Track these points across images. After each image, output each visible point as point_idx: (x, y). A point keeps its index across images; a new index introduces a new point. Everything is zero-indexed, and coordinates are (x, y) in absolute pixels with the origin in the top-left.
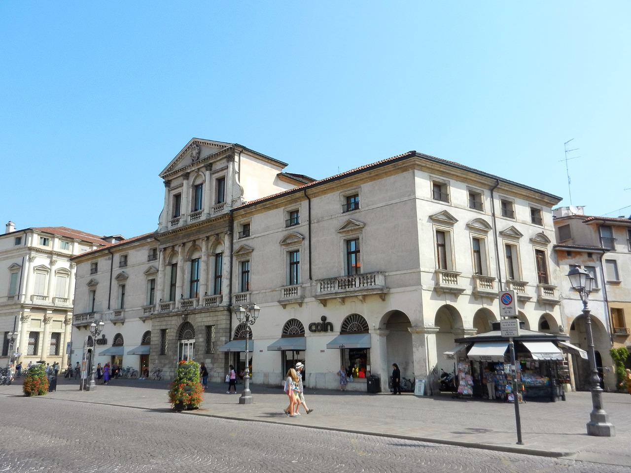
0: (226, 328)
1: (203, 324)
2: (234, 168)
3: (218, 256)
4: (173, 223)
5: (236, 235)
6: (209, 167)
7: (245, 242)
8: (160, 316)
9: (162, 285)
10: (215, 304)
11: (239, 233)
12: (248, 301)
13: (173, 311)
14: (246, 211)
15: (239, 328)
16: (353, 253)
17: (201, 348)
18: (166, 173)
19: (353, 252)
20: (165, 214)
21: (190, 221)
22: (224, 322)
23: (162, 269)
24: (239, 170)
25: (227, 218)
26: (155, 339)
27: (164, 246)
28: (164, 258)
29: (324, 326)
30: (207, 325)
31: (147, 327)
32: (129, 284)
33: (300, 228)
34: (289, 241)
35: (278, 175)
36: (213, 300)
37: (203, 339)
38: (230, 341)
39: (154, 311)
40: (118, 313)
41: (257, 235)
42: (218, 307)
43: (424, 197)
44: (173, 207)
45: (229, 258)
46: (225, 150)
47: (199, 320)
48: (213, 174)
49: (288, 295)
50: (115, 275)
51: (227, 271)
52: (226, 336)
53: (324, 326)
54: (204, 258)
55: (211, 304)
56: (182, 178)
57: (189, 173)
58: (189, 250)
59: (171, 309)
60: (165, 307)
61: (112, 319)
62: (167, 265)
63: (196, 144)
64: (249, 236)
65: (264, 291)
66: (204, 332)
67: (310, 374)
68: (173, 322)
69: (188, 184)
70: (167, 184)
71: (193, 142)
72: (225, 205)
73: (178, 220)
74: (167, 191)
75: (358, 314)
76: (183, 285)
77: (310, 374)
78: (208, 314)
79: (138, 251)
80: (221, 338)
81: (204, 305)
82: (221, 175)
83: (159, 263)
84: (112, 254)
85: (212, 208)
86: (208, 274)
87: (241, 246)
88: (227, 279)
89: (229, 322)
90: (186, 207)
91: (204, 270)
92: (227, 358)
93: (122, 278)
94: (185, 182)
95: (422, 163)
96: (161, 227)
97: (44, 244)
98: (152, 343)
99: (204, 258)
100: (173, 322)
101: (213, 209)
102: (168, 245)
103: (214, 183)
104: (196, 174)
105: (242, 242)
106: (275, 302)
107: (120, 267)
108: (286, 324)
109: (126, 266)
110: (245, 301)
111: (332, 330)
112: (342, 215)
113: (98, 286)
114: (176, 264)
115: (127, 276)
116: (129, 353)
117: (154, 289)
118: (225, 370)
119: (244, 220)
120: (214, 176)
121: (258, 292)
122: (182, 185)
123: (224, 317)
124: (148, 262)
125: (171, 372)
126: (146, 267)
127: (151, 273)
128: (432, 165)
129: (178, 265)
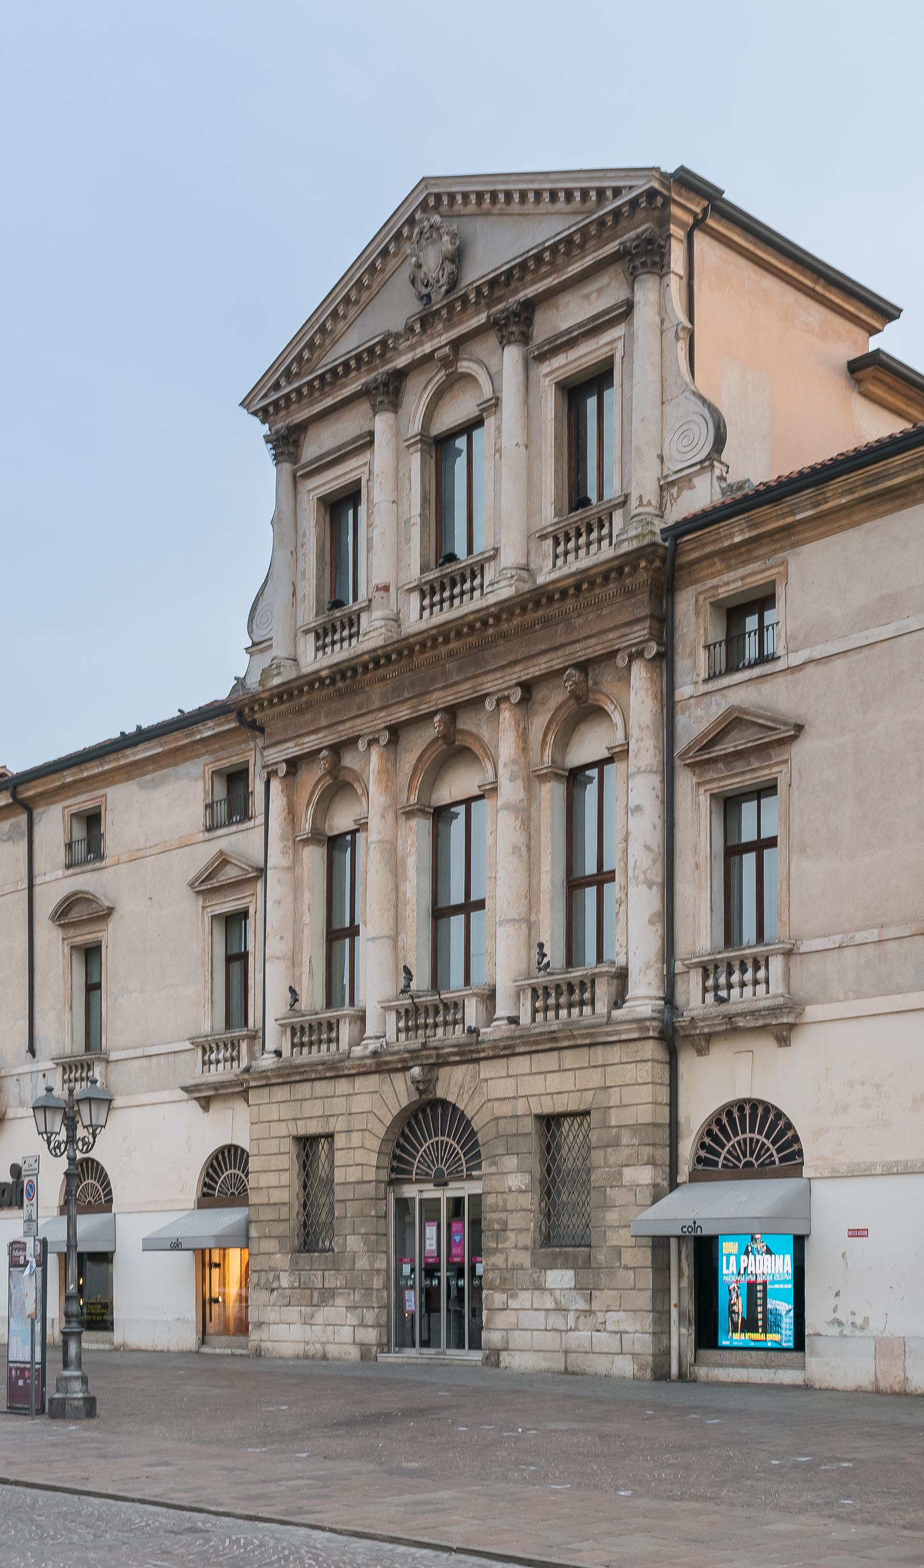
0: (655, 1125)
1: (521, 1107)
2: (663, 310)
4: (324, 634)
5: (693, 663)
6: (516, 324)
7: (742, 692)
8: (289, 1076)
9: (289, 937)
10: (587, 1010)
11: (707, 647)
12: (777, 987)
13: (357, 1051)
14: (755, 526)
15: (212, 1165)
16: (590, 884)
17: (515, 1221)
18: (277, 386)
19: (457, 909)
20: (279, 596)
21: (415, 618)
22: (646, 1093)
23: (285, 862)
24: (691, 319)
25: (643, 576)
26: (273, 1178)
27: (291, 750)
30: (302, 1132)
31: (230, 1126)
32: (114, 939)
34: (727, 747)
36: (577, 992)
37: (526, 1179)
38: (674, 1185)
40: (74, 1067)
41: (818, 652)
42: (608, 1023)
44: (320, 556)
45: (655, 781)
46: (616, 213)
47: (502, 1088)
48: (542, 357)
49: (551, 1014)
50: (48, 901)
51: (648, 848)
52: (652, 1162)
54: (510, 791)
55: (563, 1013)
56: (364, 407)
57: (400, 376)
58: (420, 759)
59: (344, 1045)
60: (306, 1032)
62: (305, 842)
63: (438, 207)
65: (873, 935)
66: (533, 1144)
68: (361, 1103)
69: (397, 432)
70: (286, 444)
71: (424, 206)
72: (618, 516)
73: (352, 621)
74: (287, 479)
75: (761, 1102)
76: (397, 934)
78: (549, 1061)
79: (154, 785)
81: (525, 1019)
83: (271, 834)
84: (27, 806)
85: (543, 537)
86: (531, 868)
87: (732, 709)
88: (650, 885)
89: (664, 1095)
90: (388, 549)
91: (405, 878)
92: (661, 1268)
93: (81, 914)
94: (382, 424)
96: (264, 661)
98: (254, 1198)
99: (510, 791)
100: (361, 1103)
101: (549, 542)
102: (311, 742)
103: (548, 406)
104: (441, 376)
105: (729, 693)
106: (174, 1088)
107: (68, 866)
109: (100, 857)
110: (761, 988)
115: (107, 904)
116: (150, 1245)
117: (98, 986)
118: (655, 1322)
119: (733, 582)
120: (545, 368)
121: (836, 940)
122: (366, 442)
123: (645, 1073)
124: (201, 836)
125: (363, 1325)
126: (203, 855)
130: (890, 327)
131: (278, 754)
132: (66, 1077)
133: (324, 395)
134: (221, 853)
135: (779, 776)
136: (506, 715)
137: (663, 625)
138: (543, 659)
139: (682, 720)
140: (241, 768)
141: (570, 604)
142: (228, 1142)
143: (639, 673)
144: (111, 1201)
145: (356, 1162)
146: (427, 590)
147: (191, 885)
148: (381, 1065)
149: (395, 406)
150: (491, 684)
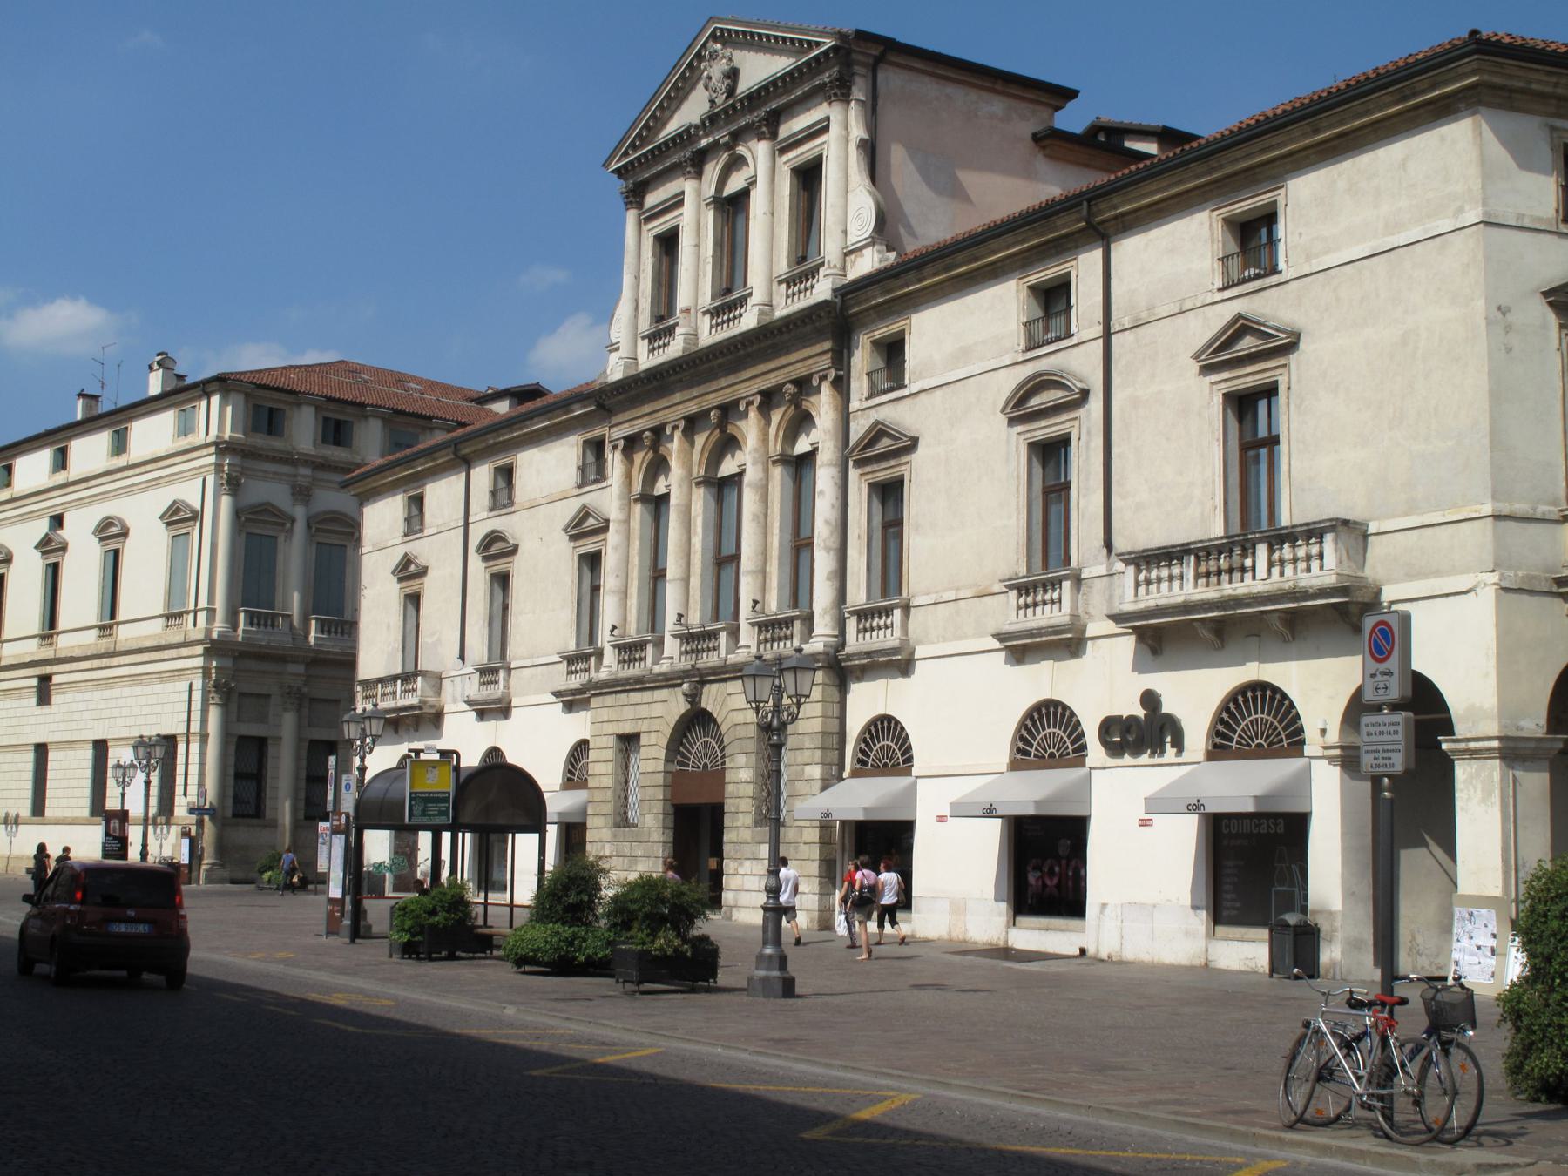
3: (801, 465)
5: (859, 386)
6: (769, 126)
12: (897, 632)
14: (1404, 99)
21: (709, 335)
28: (628, 476)
29: (1145, 732)
30: (621, 732)
31: (578, 726)
32: (519, 568)
33: (1075, 350)
34: (1036, 402)
35: (1036, 138)
38: (841, 779)
39: (597, 670)
40: (487, 673)
43: (1521, 216)
46: (816, 58)
48: (783, 151)
53: (1145, 732)
61: (472, 697)
64: (902, 386)
67: (1104, 906)
69: (699, 193)
73: (670, 331)
77: (1104, 906)
80: (807, 768)
82: (809, 156)
83: (609, 499)
87: (877, 423)
91: (755, 517)
94: (688, 186)
95: (1511, 77)
97: (270, 432)
98: (591, 784)
104: (725, 156)
108: (1018, 730)
111: (1178, 744)
112: (1219, 296)
113: (427, 580)
114: (665, 498)
116: (960, 810)
119: (883, 331)
120: (785, 158)
126: (570, 509)
127: (584, 527)
128: (1556, 85)
129: (673, 501)
130: (1071, 105)
131: (619, 433)
132: (1022, 601)
133: (656, 163)
134: (584, 506)
135: (1280, 379)
136: (753, 414)
137: (841, 357)
138: (772, 375)
139: (853, 426)
140: (1267, 211)
141: (786, 337)
142: (1047, 695)
143: (826, 389)
144: (910, 760)
145: (651, 758)
146: (715, 312)
147: (565, 530)
148: (668, 681)
149: (699, 174)
150: (745, 390)
